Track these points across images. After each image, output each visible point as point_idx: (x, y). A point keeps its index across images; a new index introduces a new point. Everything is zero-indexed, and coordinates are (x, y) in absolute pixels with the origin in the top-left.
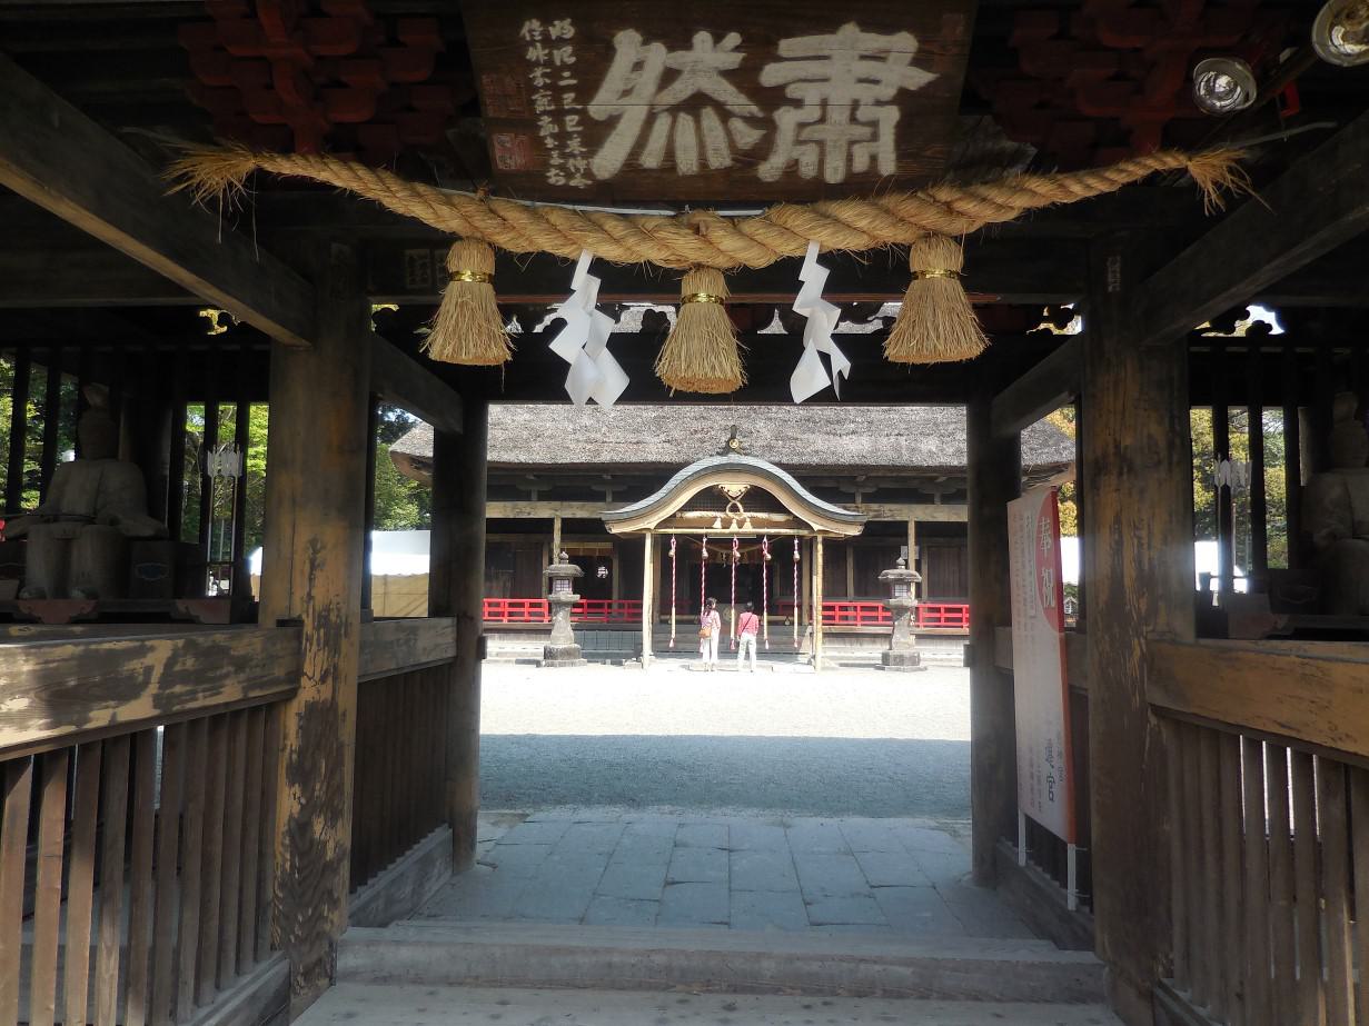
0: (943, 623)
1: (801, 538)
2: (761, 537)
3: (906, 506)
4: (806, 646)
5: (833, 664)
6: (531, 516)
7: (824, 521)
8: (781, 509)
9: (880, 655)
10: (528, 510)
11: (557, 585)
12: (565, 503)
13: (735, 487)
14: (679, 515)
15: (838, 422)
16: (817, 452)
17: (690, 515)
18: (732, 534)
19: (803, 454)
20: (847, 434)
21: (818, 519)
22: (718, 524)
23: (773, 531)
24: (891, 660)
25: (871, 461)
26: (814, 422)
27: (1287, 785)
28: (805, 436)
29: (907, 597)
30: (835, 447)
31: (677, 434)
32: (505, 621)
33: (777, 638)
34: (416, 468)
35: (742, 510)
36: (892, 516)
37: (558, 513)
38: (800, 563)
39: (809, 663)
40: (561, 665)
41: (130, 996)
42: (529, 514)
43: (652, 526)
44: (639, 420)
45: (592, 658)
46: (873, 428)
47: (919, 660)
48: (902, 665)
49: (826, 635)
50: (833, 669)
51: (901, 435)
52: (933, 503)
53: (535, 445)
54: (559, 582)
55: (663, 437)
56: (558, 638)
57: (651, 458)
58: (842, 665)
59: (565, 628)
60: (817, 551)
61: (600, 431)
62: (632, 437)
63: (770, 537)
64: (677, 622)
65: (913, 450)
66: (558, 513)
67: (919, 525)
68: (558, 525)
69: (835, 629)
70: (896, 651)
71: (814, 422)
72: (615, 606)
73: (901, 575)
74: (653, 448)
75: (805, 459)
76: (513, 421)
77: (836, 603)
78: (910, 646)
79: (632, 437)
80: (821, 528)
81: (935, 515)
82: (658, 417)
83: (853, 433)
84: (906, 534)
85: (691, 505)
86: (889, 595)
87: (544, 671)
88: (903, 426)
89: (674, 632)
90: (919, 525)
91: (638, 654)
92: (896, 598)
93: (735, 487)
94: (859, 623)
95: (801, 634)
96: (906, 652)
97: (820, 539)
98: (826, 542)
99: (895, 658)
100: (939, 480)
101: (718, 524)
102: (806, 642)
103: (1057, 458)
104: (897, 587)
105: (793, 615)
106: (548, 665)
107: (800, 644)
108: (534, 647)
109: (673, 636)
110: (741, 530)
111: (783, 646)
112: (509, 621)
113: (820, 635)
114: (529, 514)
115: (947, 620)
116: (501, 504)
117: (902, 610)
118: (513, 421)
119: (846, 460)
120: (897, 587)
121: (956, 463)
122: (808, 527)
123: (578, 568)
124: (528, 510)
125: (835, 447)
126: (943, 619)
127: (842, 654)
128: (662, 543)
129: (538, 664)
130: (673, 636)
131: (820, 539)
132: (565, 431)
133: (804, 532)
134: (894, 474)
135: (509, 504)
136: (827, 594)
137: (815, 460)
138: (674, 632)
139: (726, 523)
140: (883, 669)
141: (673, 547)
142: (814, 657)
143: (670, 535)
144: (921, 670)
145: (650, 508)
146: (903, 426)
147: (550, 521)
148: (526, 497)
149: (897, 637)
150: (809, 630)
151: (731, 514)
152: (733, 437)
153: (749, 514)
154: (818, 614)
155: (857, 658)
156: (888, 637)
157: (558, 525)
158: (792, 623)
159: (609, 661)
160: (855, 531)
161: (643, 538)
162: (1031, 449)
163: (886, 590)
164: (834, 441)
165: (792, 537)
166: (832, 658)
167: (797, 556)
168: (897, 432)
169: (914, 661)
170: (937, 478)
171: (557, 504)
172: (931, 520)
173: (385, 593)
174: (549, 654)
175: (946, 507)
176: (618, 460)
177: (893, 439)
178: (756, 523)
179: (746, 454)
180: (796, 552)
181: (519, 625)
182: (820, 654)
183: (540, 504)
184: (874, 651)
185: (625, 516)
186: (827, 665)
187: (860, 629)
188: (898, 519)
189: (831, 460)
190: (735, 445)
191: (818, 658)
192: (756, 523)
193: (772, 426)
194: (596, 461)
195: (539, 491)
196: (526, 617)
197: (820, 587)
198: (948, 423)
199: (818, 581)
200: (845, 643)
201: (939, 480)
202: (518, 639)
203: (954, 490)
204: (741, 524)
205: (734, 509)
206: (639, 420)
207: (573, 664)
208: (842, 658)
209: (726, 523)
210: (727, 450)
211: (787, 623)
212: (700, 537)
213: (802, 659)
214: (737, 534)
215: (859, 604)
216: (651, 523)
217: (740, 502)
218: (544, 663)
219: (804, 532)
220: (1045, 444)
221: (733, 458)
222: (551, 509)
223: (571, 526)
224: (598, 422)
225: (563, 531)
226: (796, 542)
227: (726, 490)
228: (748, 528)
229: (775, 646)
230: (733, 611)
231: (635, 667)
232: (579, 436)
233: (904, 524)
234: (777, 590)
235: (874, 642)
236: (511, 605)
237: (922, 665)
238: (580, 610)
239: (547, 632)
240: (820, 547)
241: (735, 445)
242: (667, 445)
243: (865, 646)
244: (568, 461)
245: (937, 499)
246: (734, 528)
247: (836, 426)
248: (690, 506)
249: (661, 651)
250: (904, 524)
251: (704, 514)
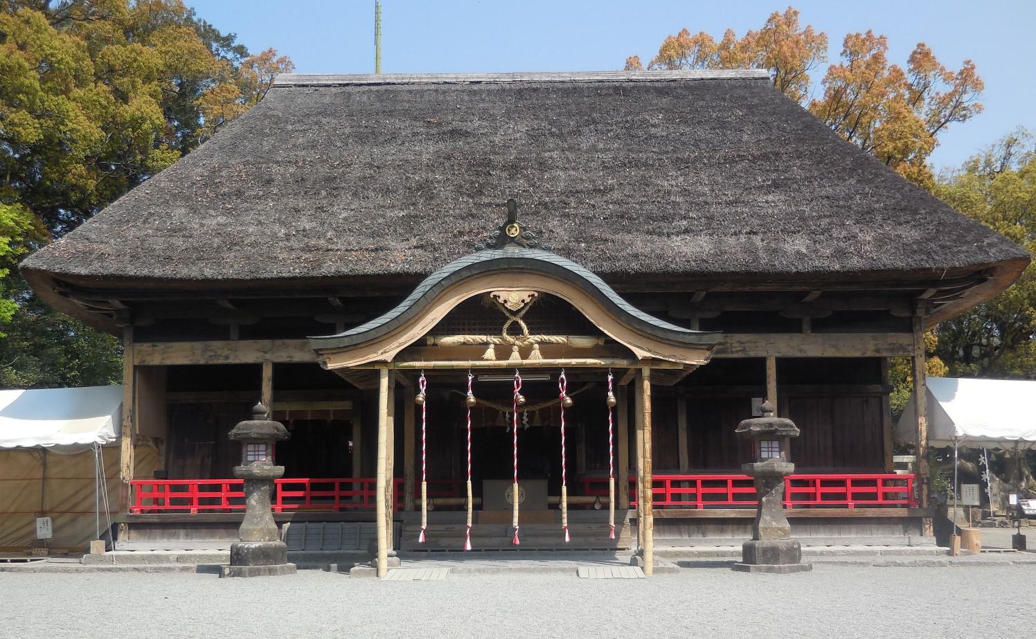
0: (819, 501)
1: (618, 373)
2: (555, 370)
3: (764, 336)
4: (628, 541)
5: (669, 563)
6: (231, 361)
7: (652, 345)
8: (587, 329)
9: (740, 548)
10: (226, 352)
11: (249, 453)
12: (278, 342)
13: (514, 296)
14: (430, 341)
15: (664, 218)
16: (636, 256)
17: (448, 340)
18: (510, 370)
19: (617, 259)
20: (678, 234)
21: (643, 342)
22: (490, 353)
23: (574, 361)
24: (758, 555)
25: (716, 268)
26: (630, 219)
27: (820, 326)
28: (618, 237)
29: (777, 460)
30: (662, 249)
31: (433, 238)
32: (194, 511)
33: (581, 527)
34: (61, 293)
35: (526, 331)
36: (744, 350)
37: (268, 356)
38: (615, 409)
39: (634, 563)
40: (253, 573)
41: (921, 297)
42: (227, 358)
43: (389, 357)
44: (381, 220)
45: (307, 562)
46: (714, 225)
47: (800, 555)
48: (777, 561)
49: (658, 522)
50: (671, 571)
51: (755, 233)
52: (800, 331)
53: (229, 256)
54: (251, 447)
55: (414, 242)
56: (249, 533)
57: (394, 268)
58: (682, 564)
59: (261, 517)
60: (642, 390)
61: (324, 235)
62: (370, 243)
63: (570, 370)
64: (570, 506)
65: (775, 251)
66: (268, 356)
67: (781, 362)
68: (267, 373)
69: (665, 514)
70: (765, 541)
71: (630, 219)
72: (356, 487)
73: (771, 425)
74: (399, 256)
75: (619, 265)
76: (202, 225)
77: (668, 477)
78: (786, 533)
79: (370, 243)
80: (648, 355)
81: (804, 347)
82: (409, 216)
83: (687, 231)
84: (763, 382)
85: (448, 325)
86: (753, 457)
87: (234, 585)
88: (756, 222)
89: (425, 520)
90: (781, 362)
91: (371, 556)
92: (762, 460)
93: (514, 296)
94: (851, 503)
95: (619, 521)
96: (781, 543)
97: (646, 372)
98: (655, 375)
99: (765, 551)
100: (809, 298)
101: (490, 353)
102: (626, 533)
103: (981, 258)
104: (764, 444)
105: (608, 495)
106: (239, 574)
107: (617, 535)
108: (217, 548)
109: (424, 526)
110: (525, 362)
111: (592, 539)
112: (283, 510)
113: (650, 519)
114: (227, 358)
115: (825, 496)
116: (186, 345)
117: (773, 478)
118: (202, 225)
119: (678, 265)
120: (764, 444)
121: (837, 267)
122: (630, 355)
123: (281, 426)
124: (226, 352)
125: (662, 249)
126: (819, 496)
127: (678, 549)
128: (403, 387)
129: (218, 570)
130: (424, 526)
131: (646, 372)
132: (274, 236)
133: (622, 363)
134: (747, 289)
135: (199, 345)
136: (657, 466)
137: (635, 266)
138: (425, 520)
139: (503, 352)
140: (747, 569)
141: (423, 389)
142: (641, 553)
143: (416, 373)
144: (804, 569)
145: (385, 330)
146: (756, 222)
147: (256, 369)
148: (221, 334)
149: (766, 521)
150: (630, 514)
151: (510, 339)
152: (511, 221)
153: (537, 338)
154: (646, 490)
155: (700, 554)
156: (750, 524)
157: (267, 373)
158: (606, 507)
159: (334, 566)
160: (698, 360)
161: (377, 375)
162: (943, 247)
163: (747, 450)
164: (659, 243)
165: (603, 372)
166: (665, 555)
167: (611, 398)
168: (748, 229)
169: (793, 555)
170: (807, 293)
171: (266, 343)
172: (798, 355)
173: (44, 478)
174: (238, 557)
175: (819, 337)
176: (345, 270)
177: (743, 239)
178: (547, 350)
179: (531, 247)
180: (610, 394)
181: (212, 517)
182: (650, 547)
183: (243, 343)
184: (732, 544)
185: (346, 342)
186: (661, 565)
187: (702, 512)
188: (752, 354)
189: (657, 266)
190: (514, 232)
191: (649, 556)
192: (547, 350)
193: (569, 224)
194: (315, 273)
195: (283, 484)
196: (224, 505)
197: (648, 446)
198: (820, 217)
199: (644, 439)
200: (681, 534)
201: (809, 298)
202: (212, 536)
203: (830, 313)
204: (525, 353)
205: (515, 330)
206: (381, 220)
207: (271, 572)
208: (677, 554)
209: (503, 352)
210: (502, 240)
211: (597, 507)
212: (464, 371)
213: (620, 557)
214: (525, 370)
215: (699, 477)
216: (388, 352)
217: (523, 318)
218: (227, 571)
219: (622, 363)
220: (961, 240)
221: (513, 251)
222: (259, 350)
223: (284, 373)
224: (323, 224)
225: (276, 387)
226: (610, 378)
227: (501, 300)
228: (536, 358)
229: (581, 540)
230: (516, 486)
231: (367, 574)
232: (294, 243)
233: (762, 362)
234: (582, 460)
235: (722, 531)
236: (202, 488)
237: (804, 561)
238: (300, 494)
239: (232, 526)
240: (647, 384)
241: (514, 232)
242: (420, 251)
243: (710, 537)
244: (274, 274)
245: (805, 326)
246: (515, 359)
247: (662, 224)
248: (446, 326)
249: (406, 549)
250: (762, 362)
251: (469, 338)
